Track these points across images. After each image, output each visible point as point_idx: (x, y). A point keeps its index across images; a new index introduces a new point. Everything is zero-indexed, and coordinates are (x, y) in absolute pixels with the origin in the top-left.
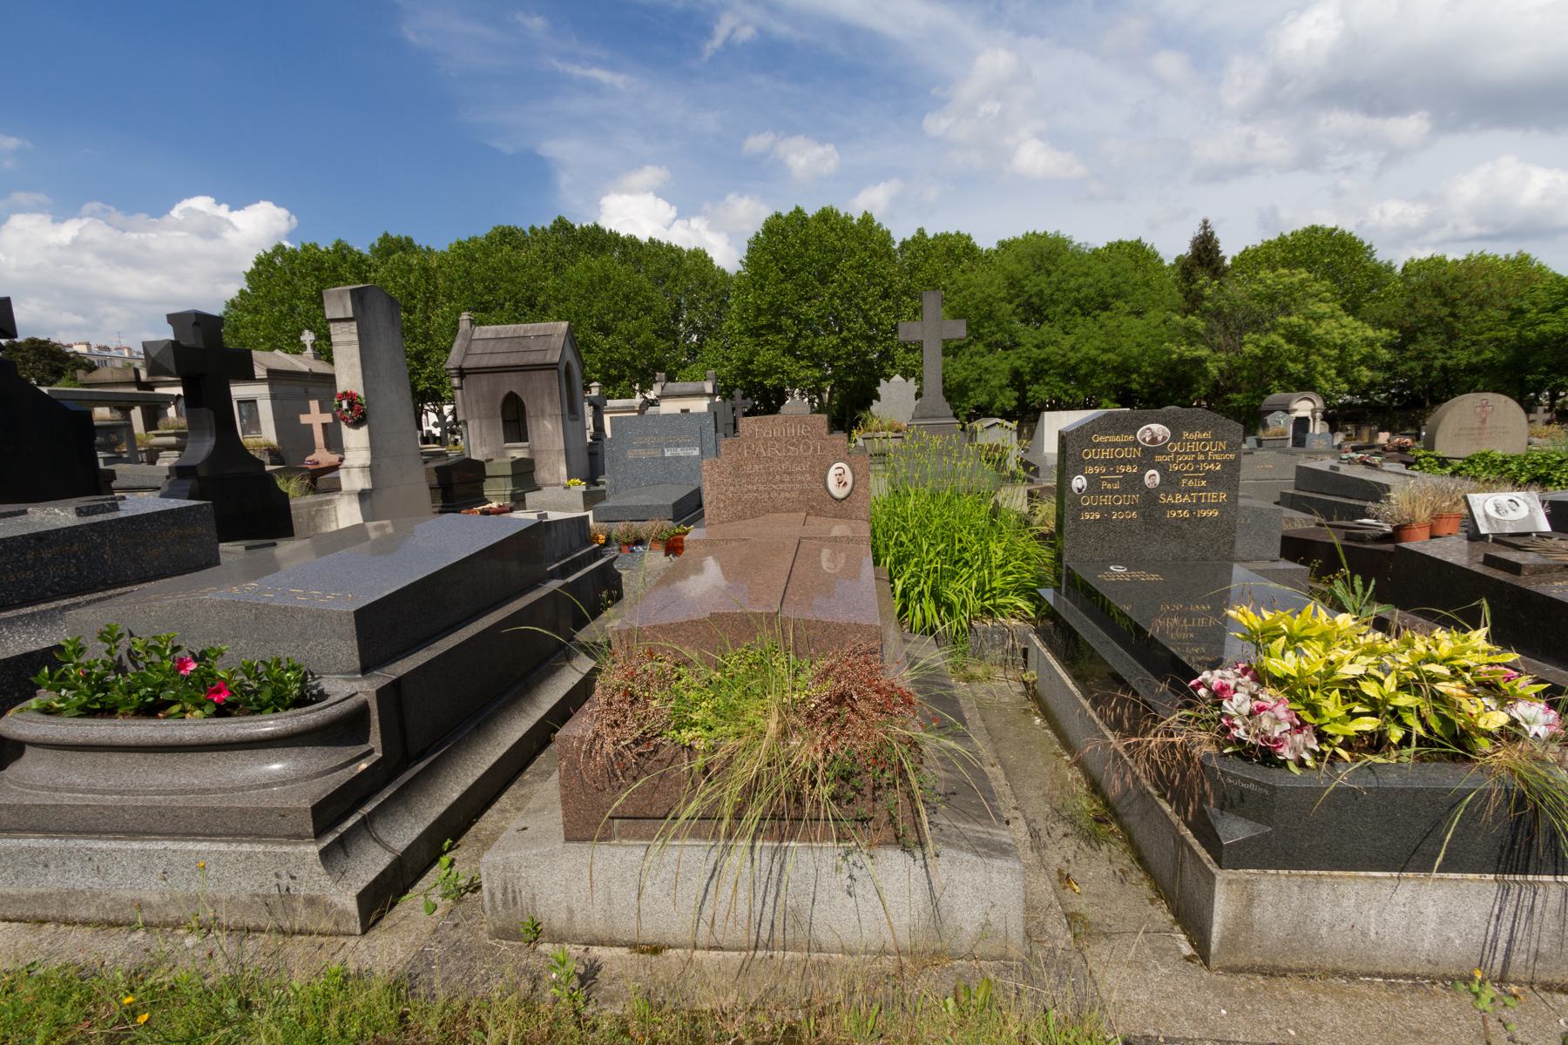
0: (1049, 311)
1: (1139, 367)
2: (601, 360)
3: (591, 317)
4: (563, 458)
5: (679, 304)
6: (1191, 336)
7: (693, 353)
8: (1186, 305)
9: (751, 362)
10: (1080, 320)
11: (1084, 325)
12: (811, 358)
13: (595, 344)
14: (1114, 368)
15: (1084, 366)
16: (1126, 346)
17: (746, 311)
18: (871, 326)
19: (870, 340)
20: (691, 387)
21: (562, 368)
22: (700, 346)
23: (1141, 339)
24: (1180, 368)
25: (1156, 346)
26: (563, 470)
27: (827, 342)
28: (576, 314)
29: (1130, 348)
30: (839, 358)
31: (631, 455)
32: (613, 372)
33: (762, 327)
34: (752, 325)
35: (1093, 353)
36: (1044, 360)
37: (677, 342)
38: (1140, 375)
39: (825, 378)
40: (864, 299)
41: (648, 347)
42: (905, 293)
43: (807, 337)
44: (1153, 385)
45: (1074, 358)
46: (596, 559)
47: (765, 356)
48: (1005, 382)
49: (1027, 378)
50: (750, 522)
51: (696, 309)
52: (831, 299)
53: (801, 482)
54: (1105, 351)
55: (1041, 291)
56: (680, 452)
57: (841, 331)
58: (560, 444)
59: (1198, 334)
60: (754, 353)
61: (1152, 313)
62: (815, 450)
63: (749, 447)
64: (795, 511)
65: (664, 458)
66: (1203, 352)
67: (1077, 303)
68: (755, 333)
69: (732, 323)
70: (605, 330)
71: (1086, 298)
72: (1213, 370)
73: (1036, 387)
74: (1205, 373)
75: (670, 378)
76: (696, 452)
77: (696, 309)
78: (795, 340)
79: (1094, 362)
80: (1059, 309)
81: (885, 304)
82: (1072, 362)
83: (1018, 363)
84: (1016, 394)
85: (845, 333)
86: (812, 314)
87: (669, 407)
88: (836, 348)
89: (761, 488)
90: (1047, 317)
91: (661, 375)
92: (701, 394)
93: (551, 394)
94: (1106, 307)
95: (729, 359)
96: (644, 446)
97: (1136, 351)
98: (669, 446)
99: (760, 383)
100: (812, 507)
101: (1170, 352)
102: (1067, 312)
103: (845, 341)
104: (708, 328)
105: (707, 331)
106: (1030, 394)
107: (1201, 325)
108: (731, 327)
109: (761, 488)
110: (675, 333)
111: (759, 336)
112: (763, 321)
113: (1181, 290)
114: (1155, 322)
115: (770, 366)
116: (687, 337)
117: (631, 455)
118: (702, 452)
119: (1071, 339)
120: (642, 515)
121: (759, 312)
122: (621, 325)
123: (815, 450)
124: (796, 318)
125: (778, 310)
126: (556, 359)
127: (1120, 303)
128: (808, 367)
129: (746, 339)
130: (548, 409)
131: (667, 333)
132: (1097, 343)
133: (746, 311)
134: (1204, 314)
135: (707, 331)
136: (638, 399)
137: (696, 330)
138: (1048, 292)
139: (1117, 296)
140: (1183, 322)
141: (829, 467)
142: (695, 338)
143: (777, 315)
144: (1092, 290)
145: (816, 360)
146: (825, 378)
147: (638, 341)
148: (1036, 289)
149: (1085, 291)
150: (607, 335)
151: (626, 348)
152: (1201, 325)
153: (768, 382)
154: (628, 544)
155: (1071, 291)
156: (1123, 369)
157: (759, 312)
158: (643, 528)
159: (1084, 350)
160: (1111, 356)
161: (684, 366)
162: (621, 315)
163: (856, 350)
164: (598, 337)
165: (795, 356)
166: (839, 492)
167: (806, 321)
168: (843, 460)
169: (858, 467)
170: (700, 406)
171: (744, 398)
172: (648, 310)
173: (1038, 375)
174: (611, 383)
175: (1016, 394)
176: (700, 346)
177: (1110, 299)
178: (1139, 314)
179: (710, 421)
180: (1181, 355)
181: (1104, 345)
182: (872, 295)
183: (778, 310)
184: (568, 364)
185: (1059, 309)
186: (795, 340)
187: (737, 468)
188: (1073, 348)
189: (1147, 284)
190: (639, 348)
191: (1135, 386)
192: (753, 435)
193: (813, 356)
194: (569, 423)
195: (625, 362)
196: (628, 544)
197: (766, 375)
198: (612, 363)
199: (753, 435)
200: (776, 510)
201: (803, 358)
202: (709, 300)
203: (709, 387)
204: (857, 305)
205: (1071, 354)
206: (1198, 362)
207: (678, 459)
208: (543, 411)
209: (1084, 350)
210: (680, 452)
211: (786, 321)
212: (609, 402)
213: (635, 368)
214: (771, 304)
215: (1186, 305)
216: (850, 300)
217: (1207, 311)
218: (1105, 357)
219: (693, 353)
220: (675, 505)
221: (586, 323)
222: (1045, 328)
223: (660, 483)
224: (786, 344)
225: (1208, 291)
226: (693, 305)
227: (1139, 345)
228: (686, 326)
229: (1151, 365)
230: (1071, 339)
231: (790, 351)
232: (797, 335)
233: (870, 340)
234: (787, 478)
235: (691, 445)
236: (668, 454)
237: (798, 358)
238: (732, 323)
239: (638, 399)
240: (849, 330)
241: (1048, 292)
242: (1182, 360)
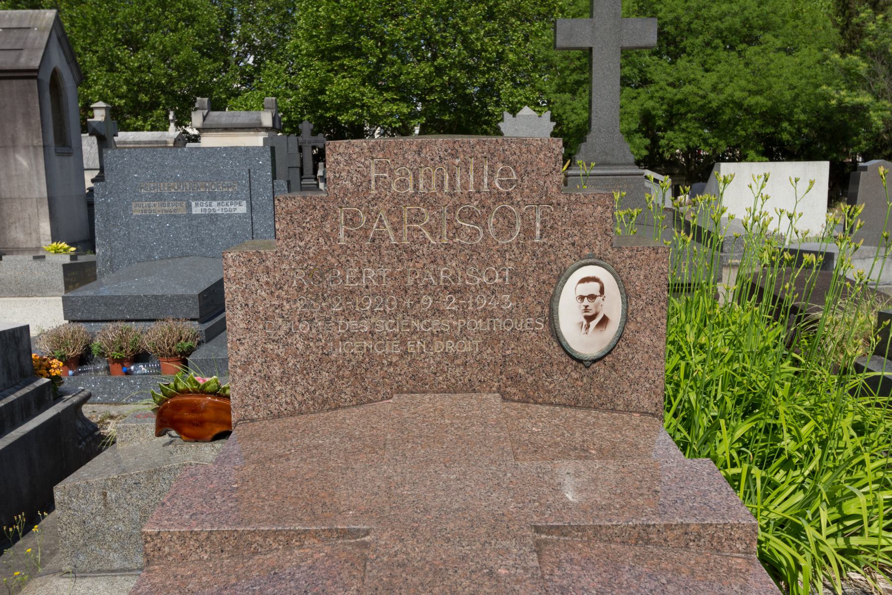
0: (686, 43)
1: (791, 113)
2: (127, 82)
3: (115, 26)
4: (45, 209)
5: (231, 16)
6: (852, 79)
7: (248, 78)
8: (843, 44)
9: (322, 92)
10: (723, 55)
11: (728, 63)
12: (399, 89)
13: (120, 60)
14: (763, 115)
15: (728, 111)
16: (776, 88)
17: (316, 27)
18: (473, 53)
19: (472, 71)
20: (242, 117)
21: (46, 77)
22: (257, 70)
23: (794, 81)
24: (838, 117)
25: (810, 89)
26: (45, 227)
27: (417, 70)
28: (95, 21)
29: (781, 90)
30: (431, 90)
31: (137, 210)
32: (144, 98)
33: (337, 48)
34: (323, 45)
35: (738, 94)
36: (680, 102)
37: (227, 63)
38: (791, 123)
39: (414, 115)
40: (464, 19)
41: (189, 68)
42: (513, 14)
43: (393, 63)
44: (807, 136)
45: (715, 100)
46: (41, 409)
47: (340, 85)
48: (634, 126)
49: (660, 122)
50: (351, 417)
51: (253, 22)
52: (423, 17)
53: (488, 314)
54: (751, 93)
55: (677, 18)
56: (217, 208)
57: (434, 57)
58: (41, 190)
59: (859, 77)
60: (325, 81)
61: (805, 51)
62: (528, 232)
63: (351, 220)
64: (469, 388)
65: (191, 217)
66: (866, 99)
67: (719, 33)
68: (327, 55)
69: (298, 42)
70: (134, 43)
71: (729, 29)
72: (875, 118)
73: (670, 134)
74: (866, 123)
75: (217, 106)
76: (242, 209)
77: (253, 22)
78: (378, 67)
79: (739, 105)
80: (699, 41)
81: (489, 26)
82: (714, 105)
83: (650, 104)
84: (647, 141)
85: (440, 60)
86: (400, 34)
87: (209, 141)
88: (429, 78)
89: (384, 327)
90: (684, 50)
91: (202, 101)
92: (256, 128)
93: (27, 115)
94: (751, 40)
95: (293, 87)
96: (158, 197)
97: (788, 95)
98: (198, 197)
99: (334, 119)
100: (515, 379)
101: (826, 98)
102: (708, 44)
103: (440, 71)
104: (268, 47)
105: (265, 51)
106: (663, 142)
107: (863, 67)
108: (296, 47)
109: (384, 327)
110: (226, 52)
111: (331, 59)
112: (338, 40)
113: (836, 25)
114: (810, 61)
115: (346, 97)
116: (242, 57)
117: (137, 210)
118: (251, 208)
119: (712, 77)
120: (148, 310)
121: (333, 28)
122: (155, 38)
123: (528, 232)
124: (380, 38)
125: (355, 27)
126: (35, 63)
127: (768, 37)
128: (393, 101)
129: (316, 63)
130: (22, 138)
131: (215, 51)
132: (743, 83)
133: (316, 27)
134: (865, 54)
135: (265, 51)
136: (173, 132)
137: (252, 49)
138: (685, 19)
139: (765, 28)
140: (843, 62)
141: (562, 276)
142: (251, 60)
143: (356, 35)
144: (737, 20)
145: (404, 93)
146: (414, 115)
147: (177, 59)
148: (671, 16)
149: (728, 21)
150: (136, 50)
151: (161, 68)
152: (863, 67)
153: (343, 118)
154: (121, 361)
155: (713, 19)
156: (773, 116)
157: (333, 28)
158: (151, 335)
159: (728, 91)
160: (759, 99)
161: (236, 94)
162: (154, 24)
163: (454, 85)
164: (123, 52)
165: (377, 87)
166: (585, 342)
167: (392, 42)
168: (598, 260)
169: (637, 278)
170: (257, 140)
171: (314, 133)
172: (190, 21)
173: (673, 119)
174: (134, 109)
175: (647, 141)
176: (257, 70)
177: (757, 32)
178: (789, 52)
179: (265, 161)
180: (840, 102)
181: (751, 87)
182: (473, 14)
183: (355, 27)
184: (55, 74)
185: (699, 41)
186: (378, 67)
187: (319, 273)
188: (714, 88)
189: (796, 16)
190: (177, 69)
191: (785, 136)
192: (362, 188)
193: (399, 89)
194: (56, 160)
195: (160, 86)
196: (121, 361)
197: (341, 109)
198: (141, 87)
199: (362, 188)
200: (419, 384)
201: (388, 89)
202: (268, 13)
203: (267, 119)
204: (454, 26)
205: (712, 96)
206: (859, 110)
207: (213, 218)
208: (14, 140)
209: (728, 91)
210: (217, 208)
211: (367, 42)
212: (122, 136)
213: (173, 93)
214: (348, 20)
215: (843, 44)
216: (446, 19)
217: (869, 49)
218: (752, 100)
219: (248, 78)
220: (199, 295)
221: (108, 33)
222: (682, 62)
223: (184, 255)
224: (367, 71)
225: (871, 27)
226: (248, 17)
227: (792, 87)
228: (240, 44)
229: (804, 111)
230: (712, 77)
231: (371, 79)
232: (380, 61)
233: (472, 71)
234: (449, 303)
235: (235, 198)
236: (196, 210)
237: (381, 90)
238: (298, 42)
239: (173, 132)
240: (445, 57)
241: (685, 19)
242: (841, 107)
